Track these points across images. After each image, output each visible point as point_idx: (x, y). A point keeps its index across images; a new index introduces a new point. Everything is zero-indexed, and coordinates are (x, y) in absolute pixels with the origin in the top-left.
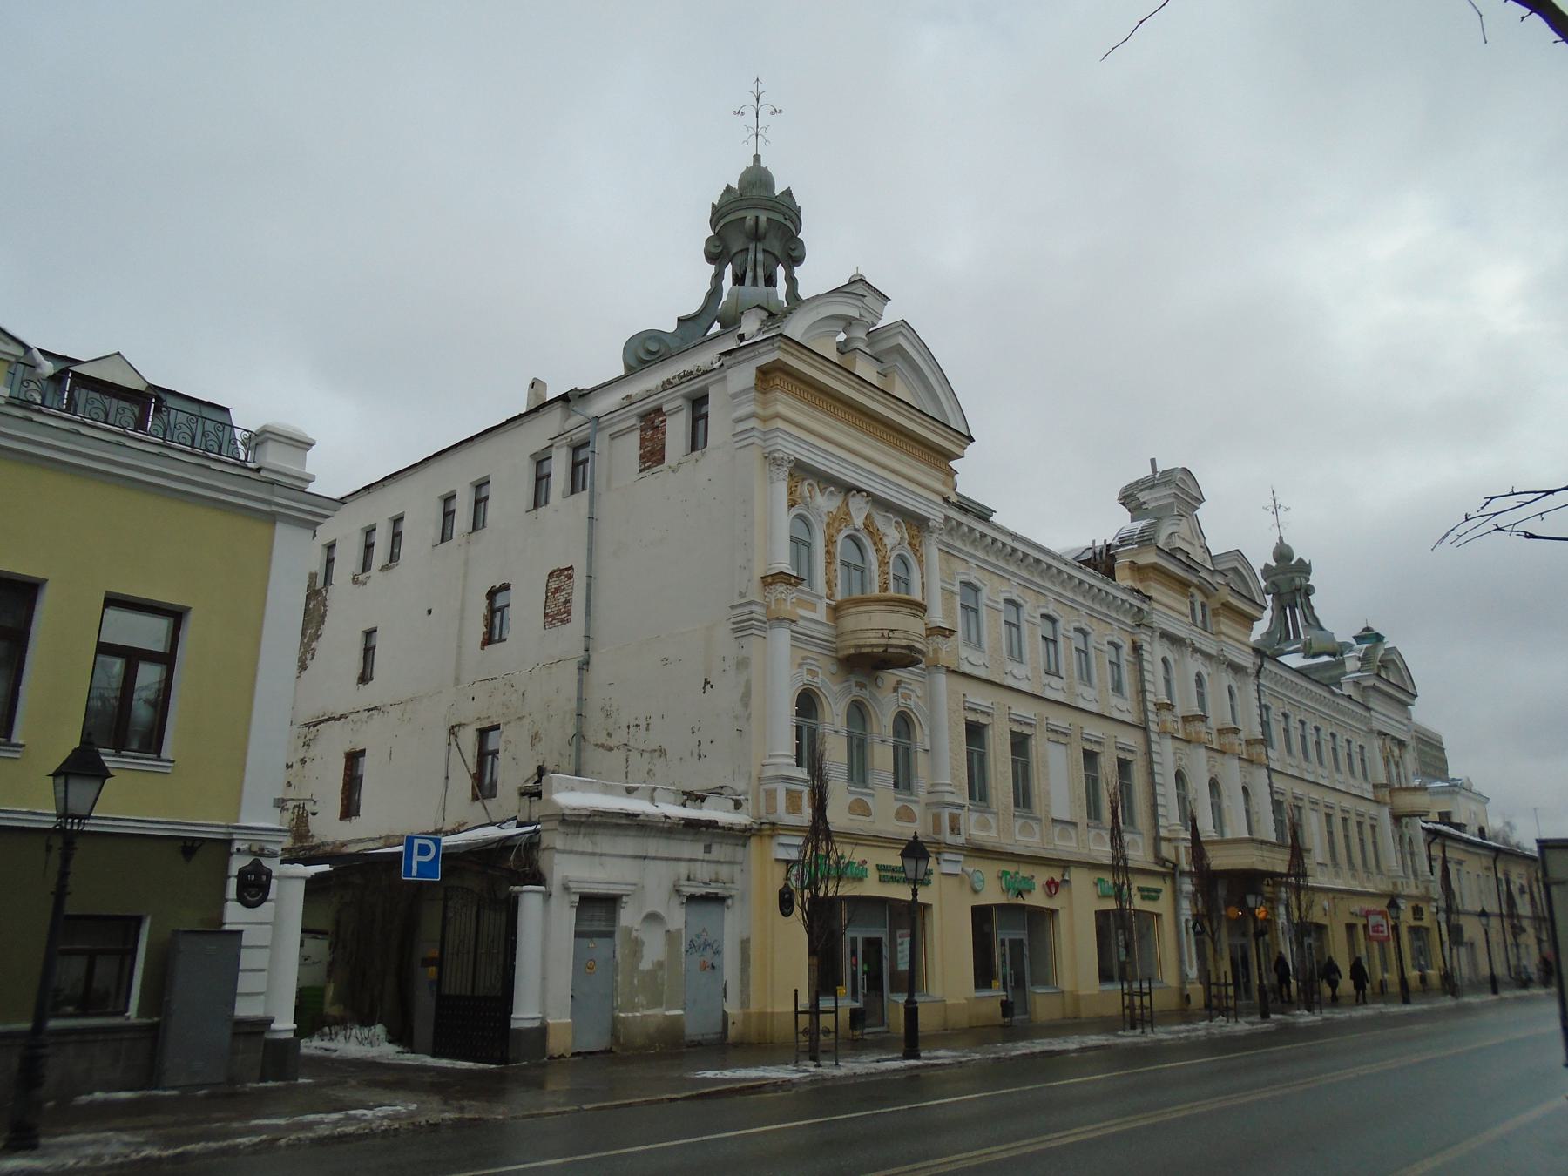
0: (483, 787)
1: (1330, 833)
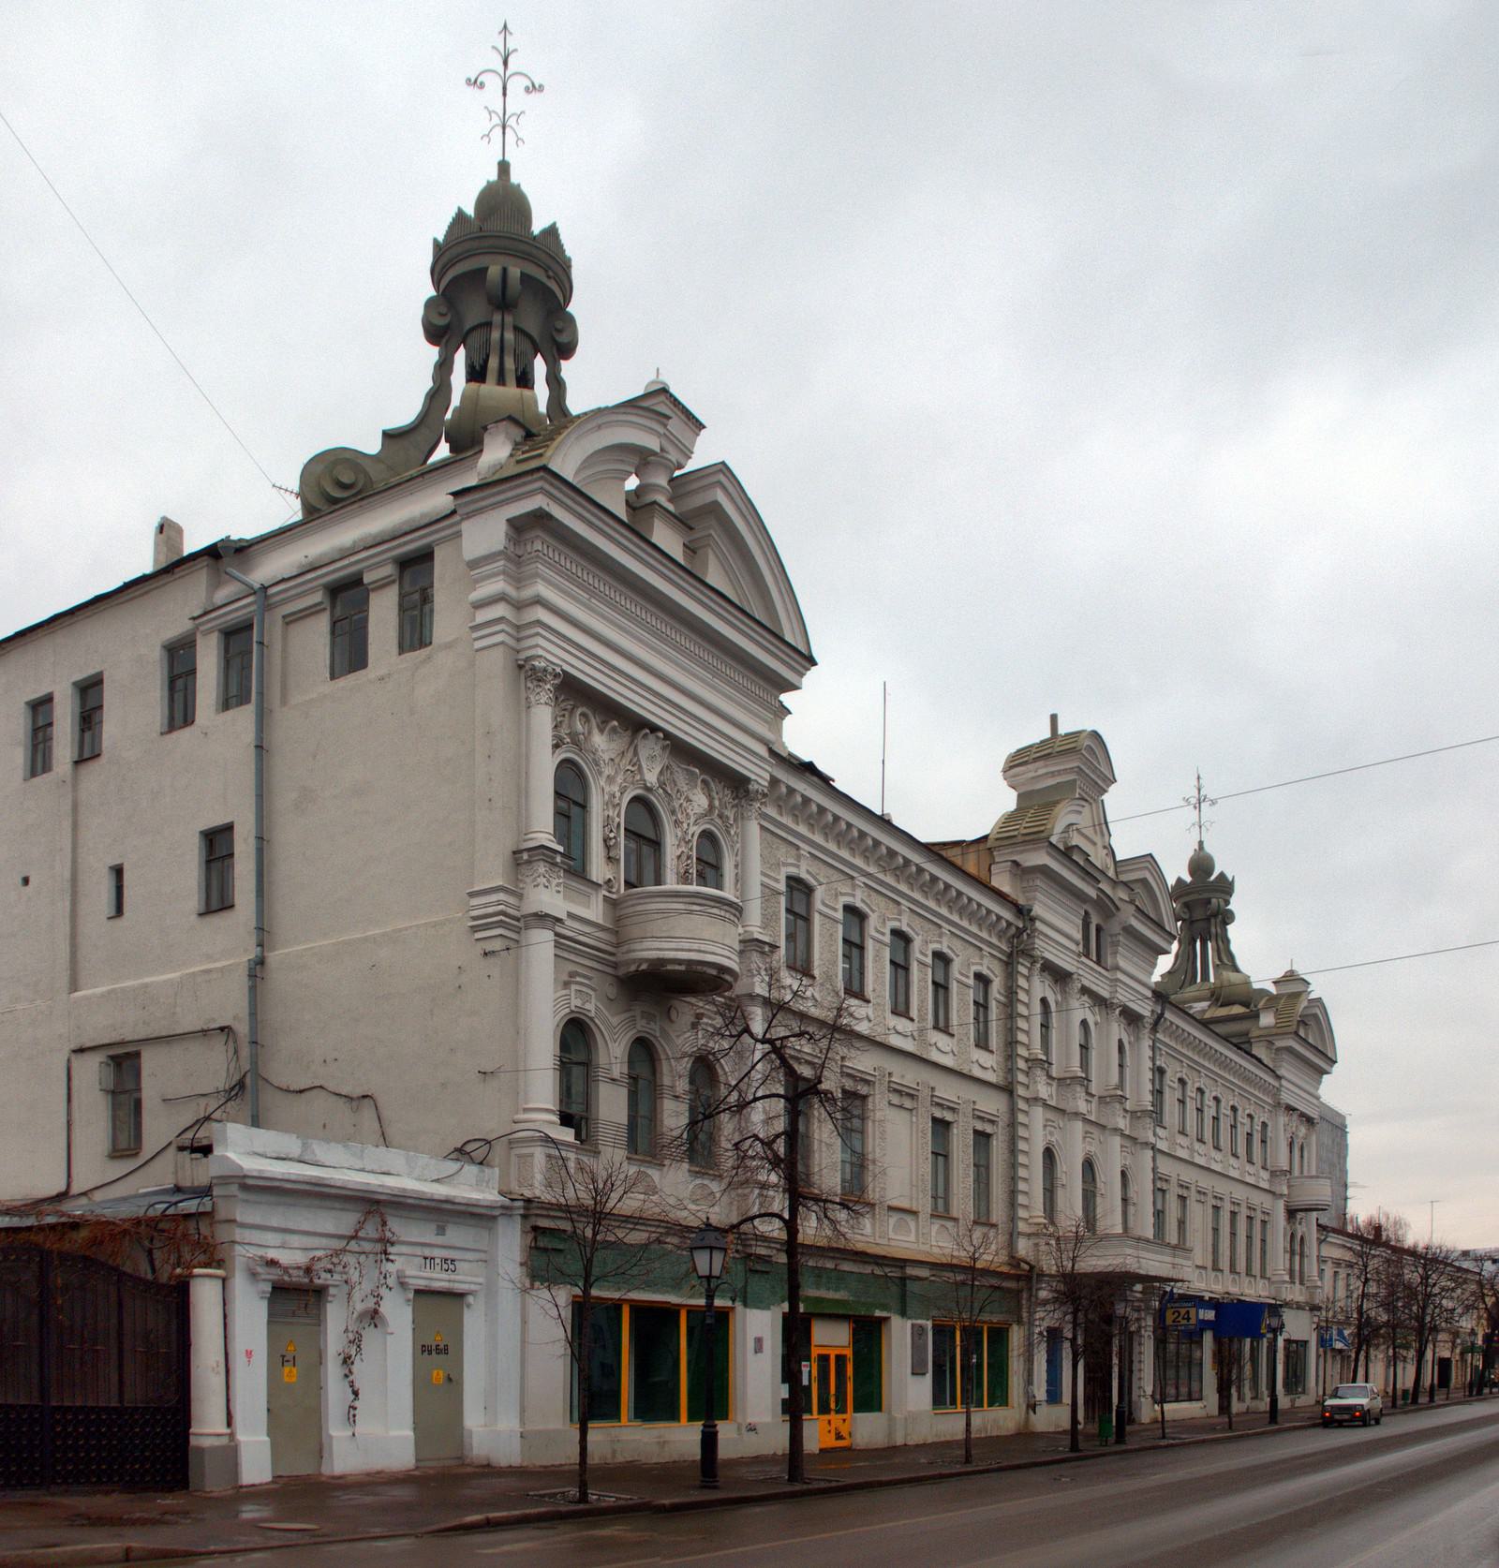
0: (126, 1144)
1: (1216, 1230)
